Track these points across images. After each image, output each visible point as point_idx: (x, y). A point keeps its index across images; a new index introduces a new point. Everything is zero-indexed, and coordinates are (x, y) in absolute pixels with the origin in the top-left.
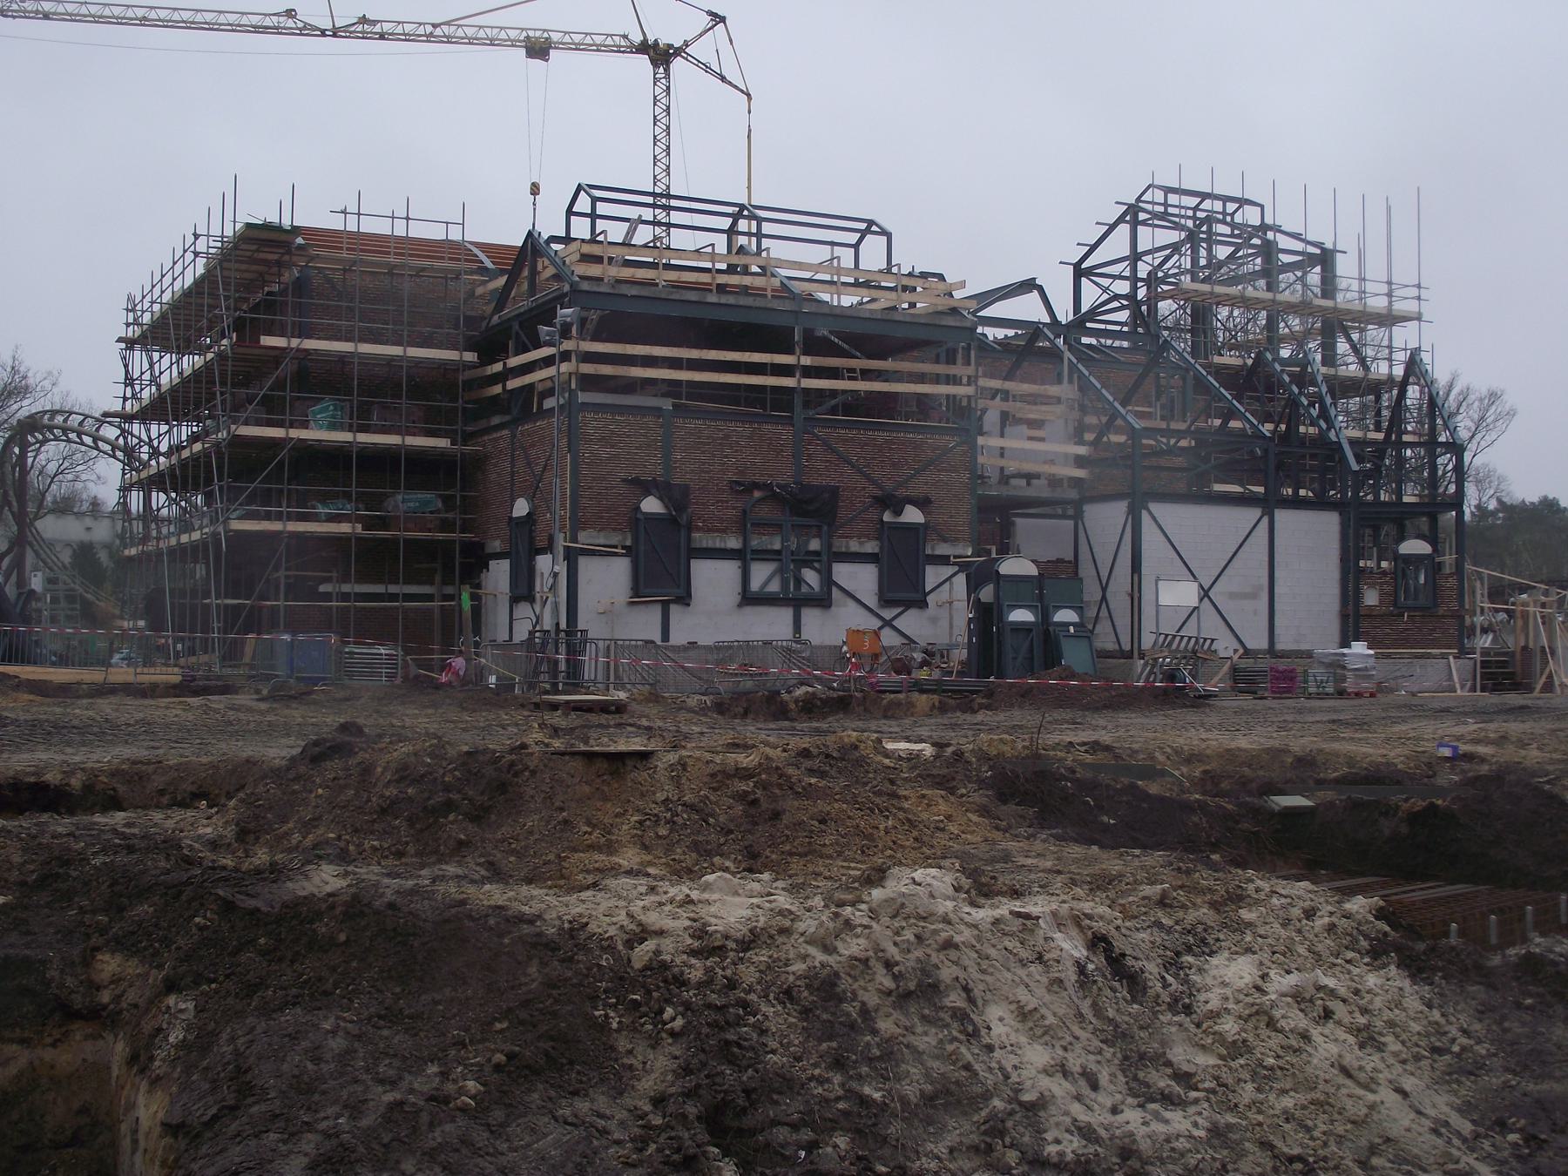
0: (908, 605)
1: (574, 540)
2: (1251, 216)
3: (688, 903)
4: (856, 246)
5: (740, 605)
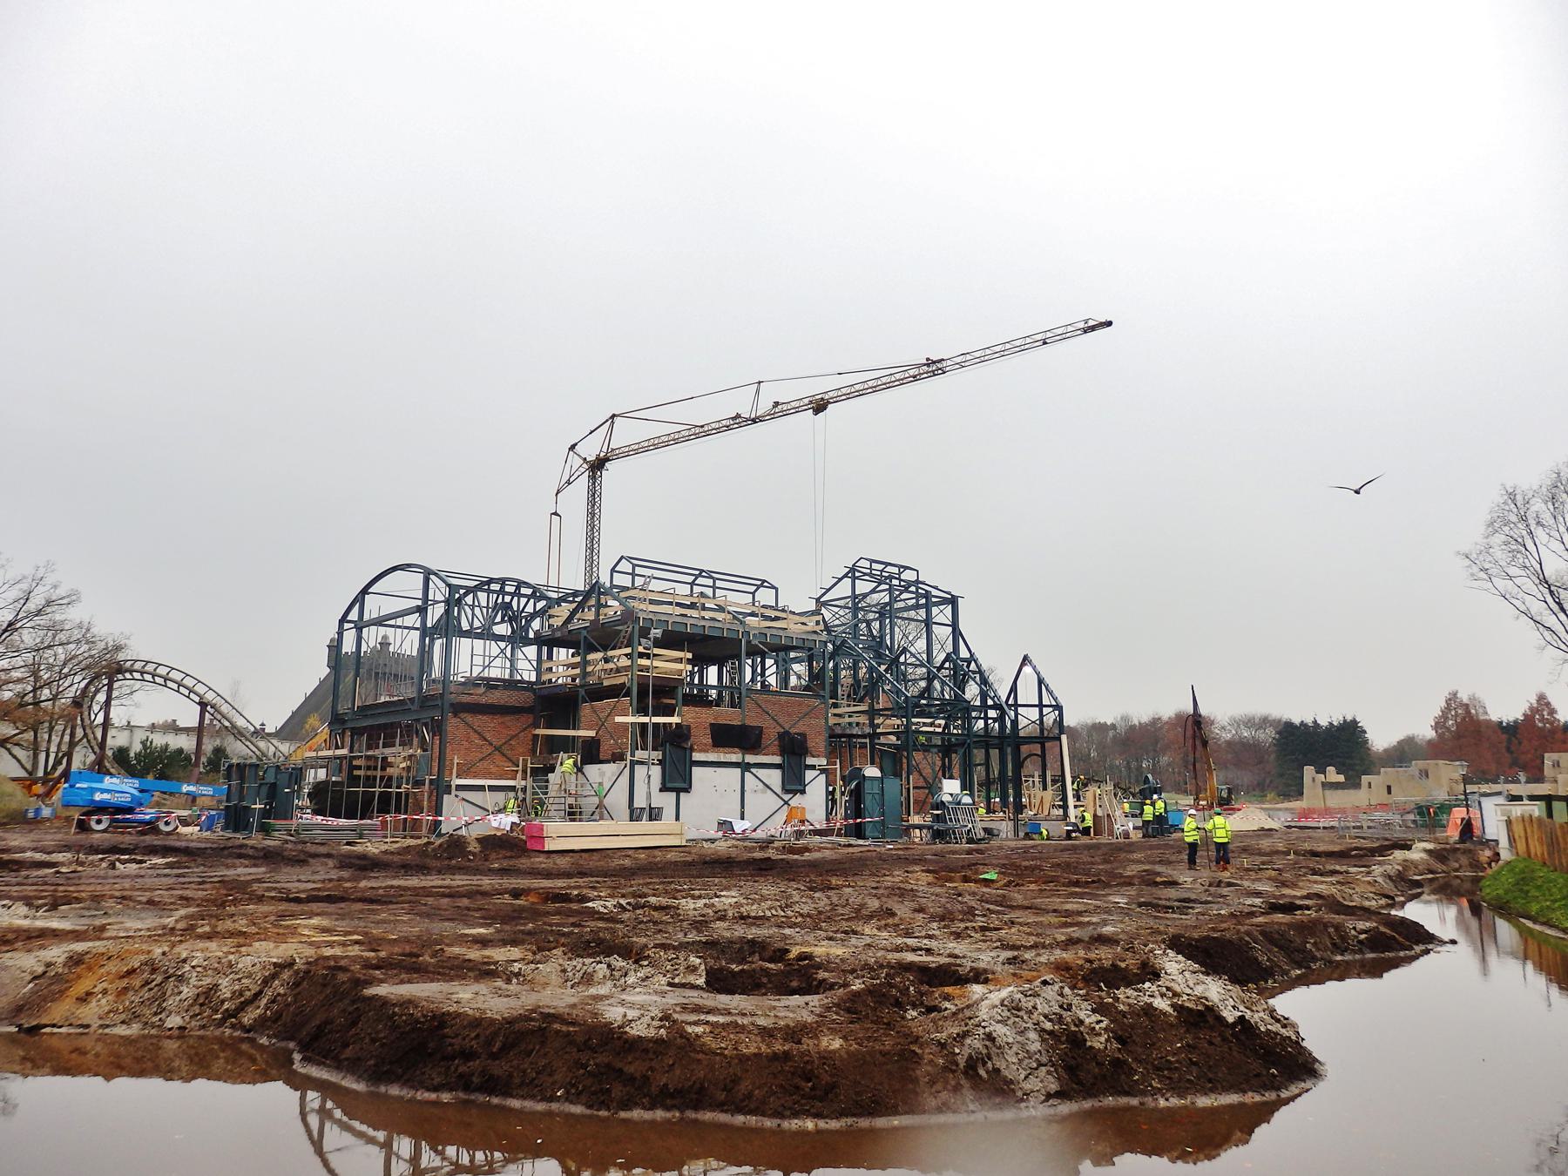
0: (794, 792)
1: (633, 756)
2: (909, 576)
3: (1022, 1032)
4: (753, 594)
5: (661, 790)
